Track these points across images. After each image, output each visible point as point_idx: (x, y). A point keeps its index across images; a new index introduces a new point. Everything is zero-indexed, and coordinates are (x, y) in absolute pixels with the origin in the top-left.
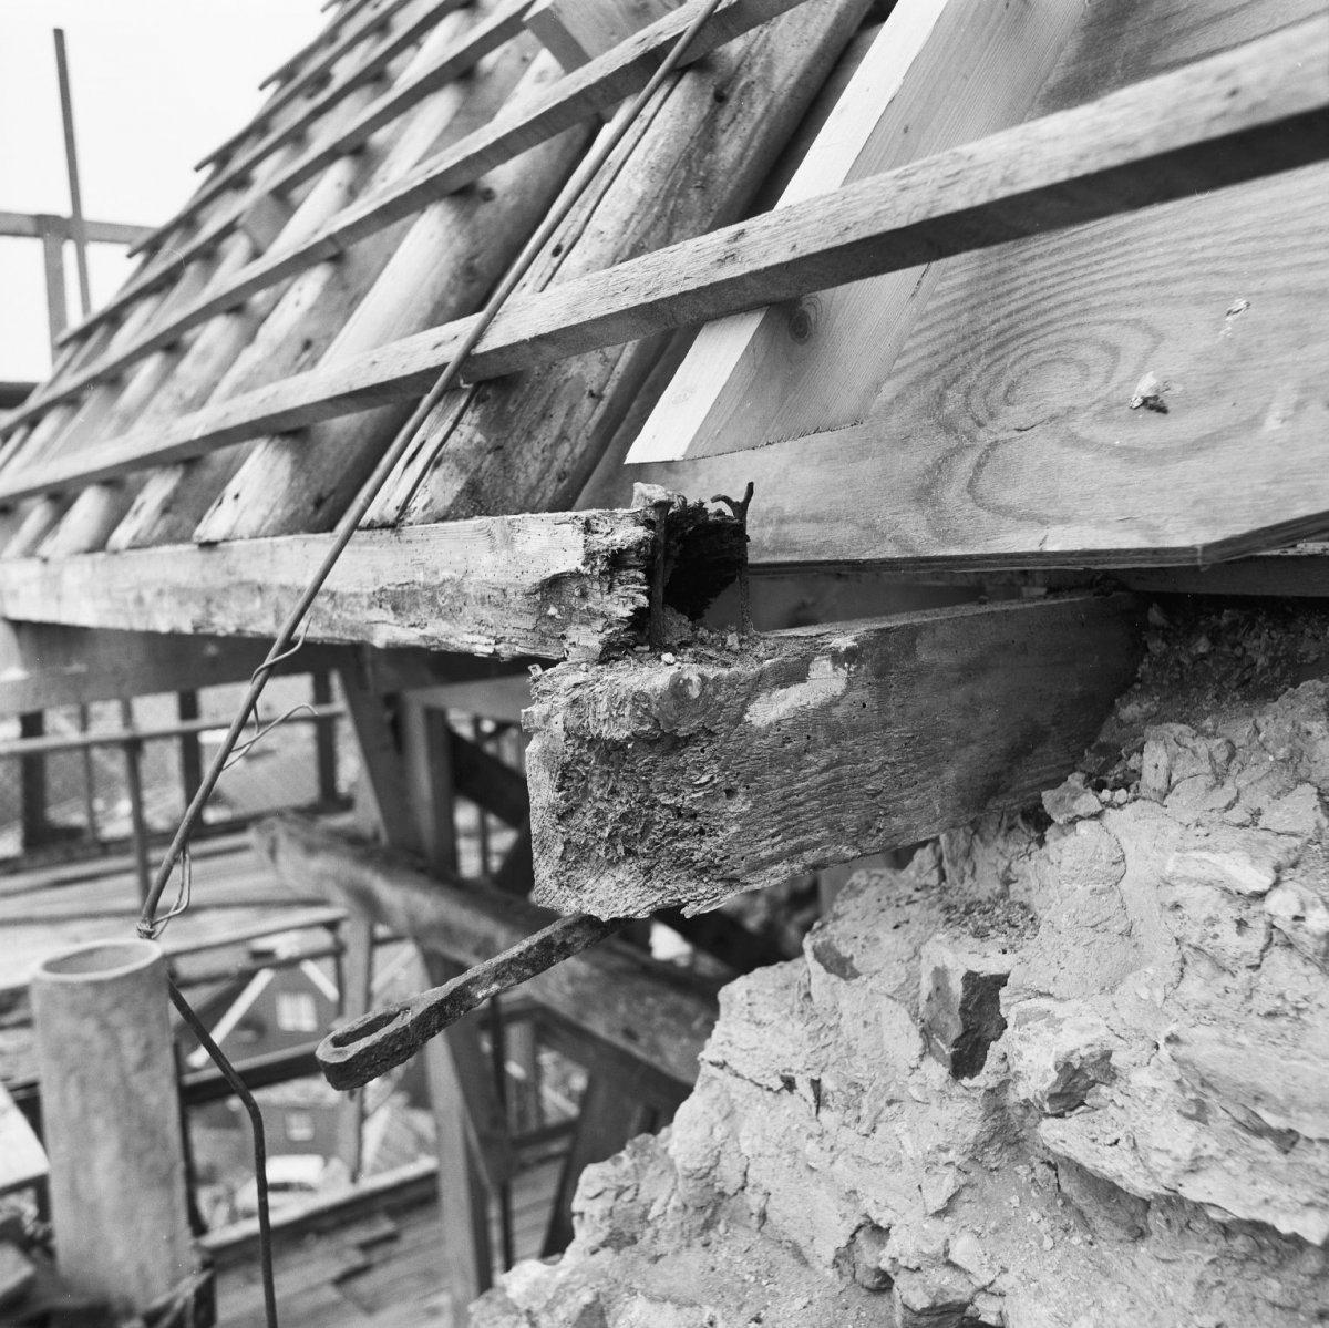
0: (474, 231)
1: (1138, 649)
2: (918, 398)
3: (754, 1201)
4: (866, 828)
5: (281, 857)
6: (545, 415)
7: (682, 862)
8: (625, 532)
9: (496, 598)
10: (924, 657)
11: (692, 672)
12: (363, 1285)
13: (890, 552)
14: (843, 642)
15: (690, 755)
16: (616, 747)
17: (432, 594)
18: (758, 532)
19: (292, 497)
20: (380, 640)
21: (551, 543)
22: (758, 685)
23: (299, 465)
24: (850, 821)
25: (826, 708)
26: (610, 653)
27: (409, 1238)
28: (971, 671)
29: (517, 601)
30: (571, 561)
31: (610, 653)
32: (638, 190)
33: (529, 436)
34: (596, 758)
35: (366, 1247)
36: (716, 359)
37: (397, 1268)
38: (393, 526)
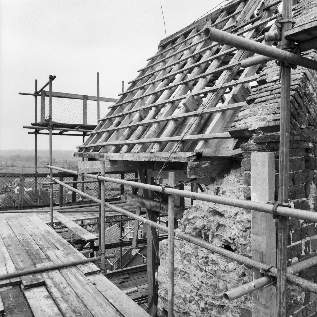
0: (176, 124)
1: (233, 165)
2: (215, 145)
3: (200, 208)
4: (210, 175)
5: (223, 147)
6: (187, 144)
7: (198, 175)
8: (194, 154)
9: (184, 158)
10: (215, 163)
11: (199, 163)
12: (124, 284)
13: (212, 156)
14: (209, 162)
15: (198, 168)
16: (194, 167)
17: (178, 158)
18: (203, 154)
19: (159, 149)
20: (172, 161)
21: (189, 154)
22: (203, 164)
23: (160, 146)
24: (209, 174)
25: (207, 166)
26: (193, 162)
27: (131, 278)
28: (219, 165)
29: (186, 158)
30: (191, 155)
31: (193, 162)
32: (194, 126)
33: (185, 146)
34: (192, 168)
35: (124, 279)
36: (201, 143)
37: (130, 282)
38: (175, 152)
